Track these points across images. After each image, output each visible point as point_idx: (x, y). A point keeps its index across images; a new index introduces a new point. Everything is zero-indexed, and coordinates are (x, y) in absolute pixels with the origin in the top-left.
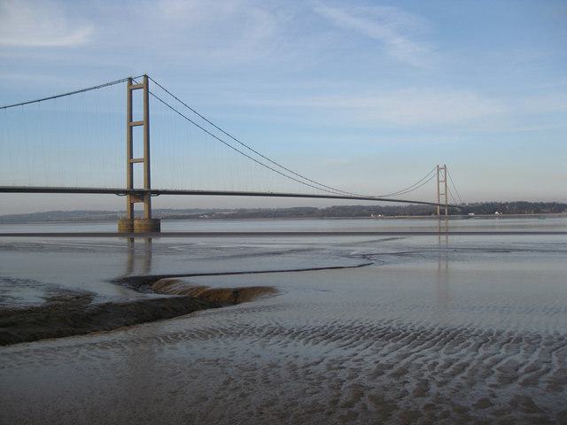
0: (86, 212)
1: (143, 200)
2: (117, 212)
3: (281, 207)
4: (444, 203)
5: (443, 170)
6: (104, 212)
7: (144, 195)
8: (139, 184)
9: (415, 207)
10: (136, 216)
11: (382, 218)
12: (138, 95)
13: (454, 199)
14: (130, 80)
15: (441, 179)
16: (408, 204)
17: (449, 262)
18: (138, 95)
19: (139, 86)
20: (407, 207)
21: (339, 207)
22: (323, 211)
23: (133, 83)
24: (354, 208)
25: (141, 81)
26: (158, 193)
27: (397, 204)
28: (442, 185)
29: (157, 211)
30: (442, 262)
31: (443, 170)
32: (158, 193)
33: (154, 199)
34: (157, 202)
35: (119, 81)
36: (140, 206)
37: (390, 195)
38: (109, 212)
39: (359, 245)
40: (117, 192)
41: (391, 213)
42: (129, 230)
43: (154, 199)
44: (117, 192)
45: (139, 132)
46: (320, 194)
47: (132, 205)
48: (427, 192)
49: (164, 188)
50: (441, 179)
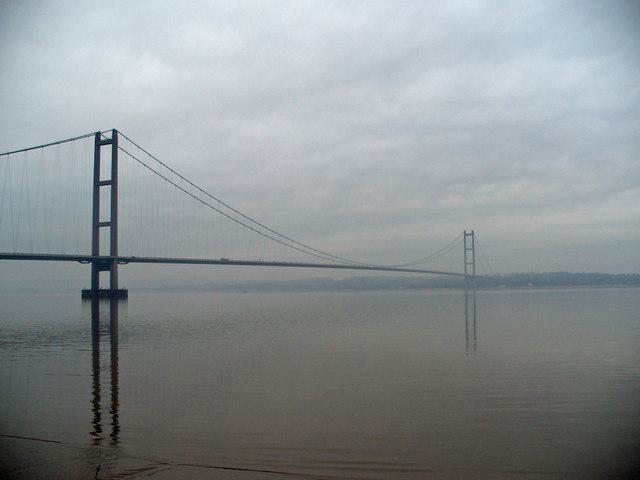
1: (109, 270)
5: (108, 188)
8: (105, 251)
12: (106, 151)
14: (98, 135)
18: (106, 151)
25: (109, 136)
26: (127, 260)
31: (108, 188)
32: (127, 260)
33: (121, 268)
40: (80, 259)
42: (93, 295)
43: (121, 268)
44: (80, 259)
45: (105, 215)
46: (322, 263)
50: (469, 246)
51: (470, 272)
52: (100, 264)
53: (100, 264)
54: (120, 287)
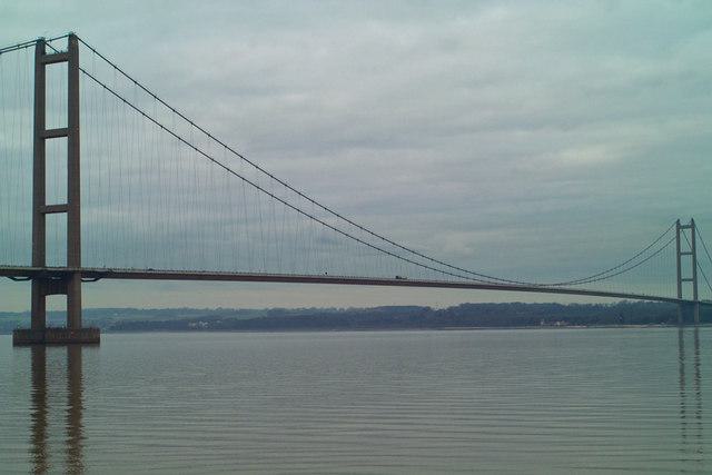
2: (17, 315)
4: (692, 299)
8: (56, 258)
11: (561, 326)
12: (57, 74)
15: (685, 247)
17: (27, 322)
18: (57, 74)
20: (635, 304)
22: (440, 313)
23: (48, 51)
24: (575, 308)
25: (62, 46)
26: (96, 275)
27: (609, 301)
28: (687, 261)
29: (94, 312)
30: (62, 322)
32: (96, 275)
34: (94, 296)
36: (56, 303)
37: (585, 281)
40: (685, 254)
44: (685, 254)
49: (110, 266)
50: (685, 247)
51: (688, 295)
52: (45, 281)
53: (45, 281)
54: (86, 321)
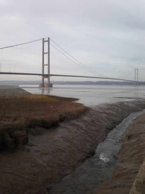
0: (16, 81)
3: (81, 81)
6: (23, 81)
7: (48, 76)
8: (46, 72)
9: (125, 82)
10: (45, 82)
12: (46, 44)
13: (140, 80)
16: (123, 81)
18: (46, 44)
19: (46, 41)
21: (101, 81)
22: (95, 82)
25: (47, 39)
26: (52, 75)
28: (136, 75)
29: (45, 81)
32: (52, 75)
33: (51, 77)
35: (25, 43)
36: (46, 80)
38: (24, 81)
39: (112, 91)
41: (30, 84)
43: (51, 77)
45: (46, 56)
47: (43, 79)
48: (132, 78)
53: (44, 76)
54: (50, 83)
